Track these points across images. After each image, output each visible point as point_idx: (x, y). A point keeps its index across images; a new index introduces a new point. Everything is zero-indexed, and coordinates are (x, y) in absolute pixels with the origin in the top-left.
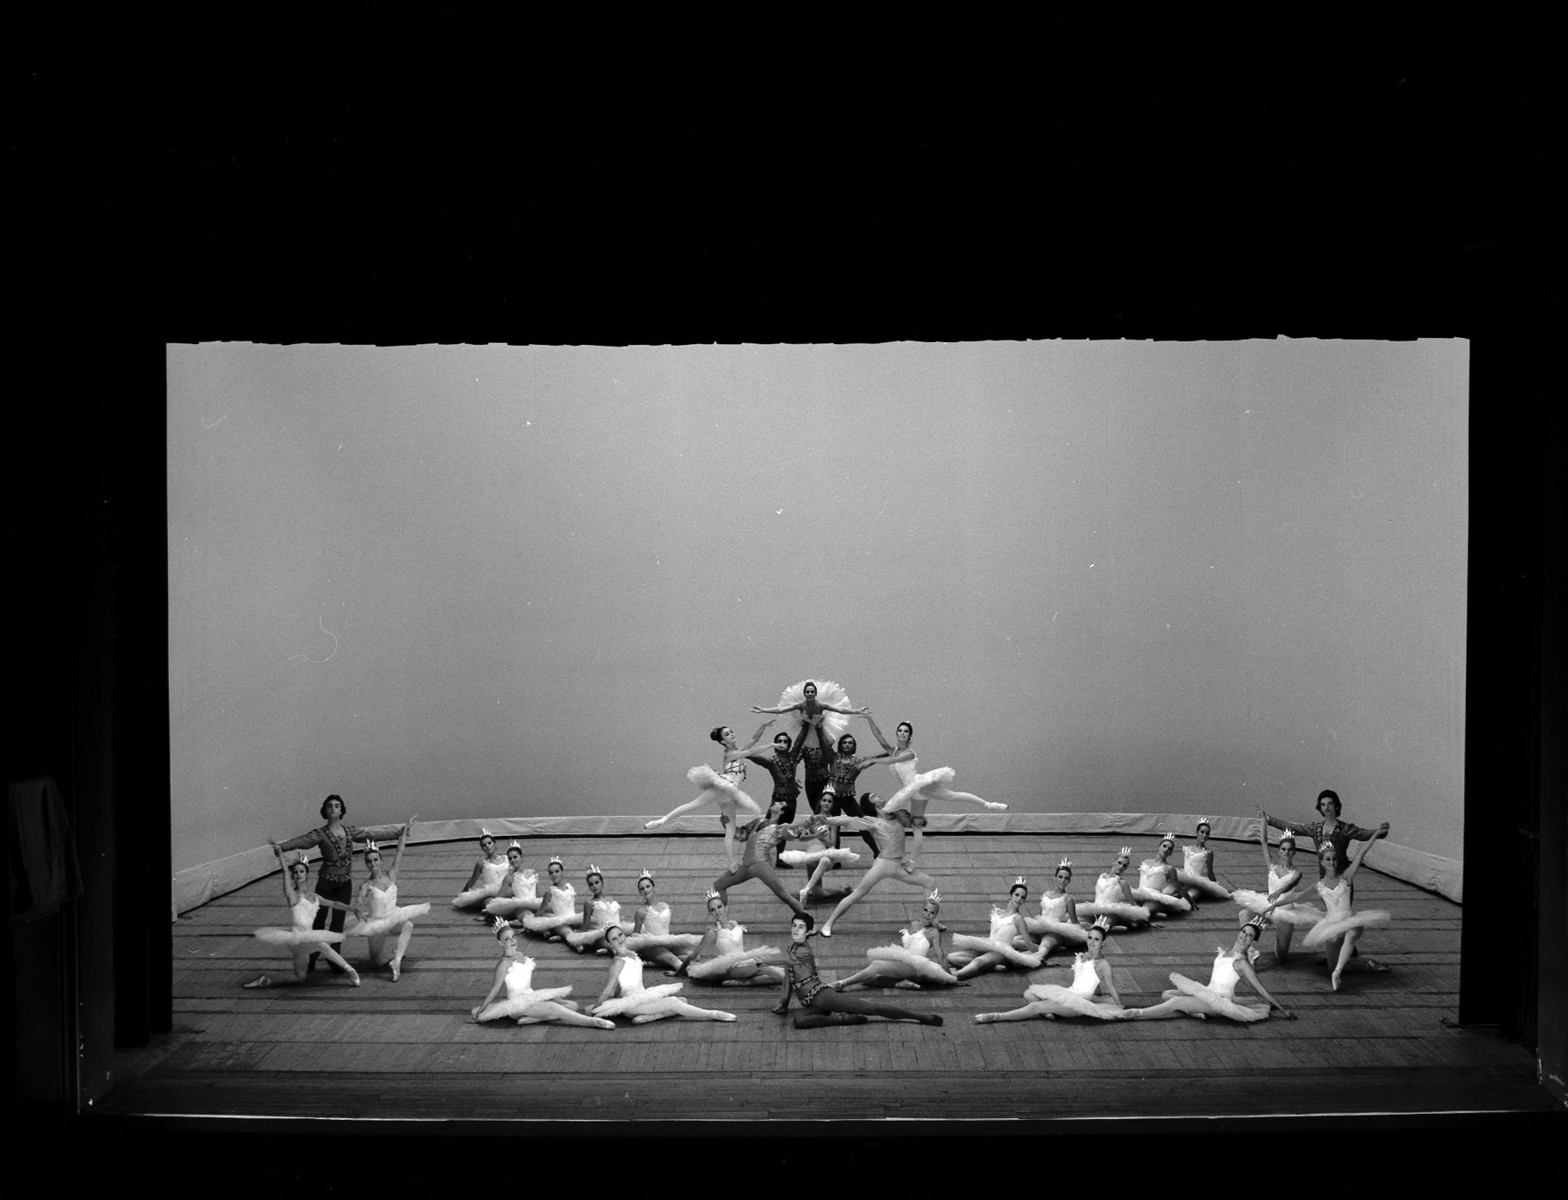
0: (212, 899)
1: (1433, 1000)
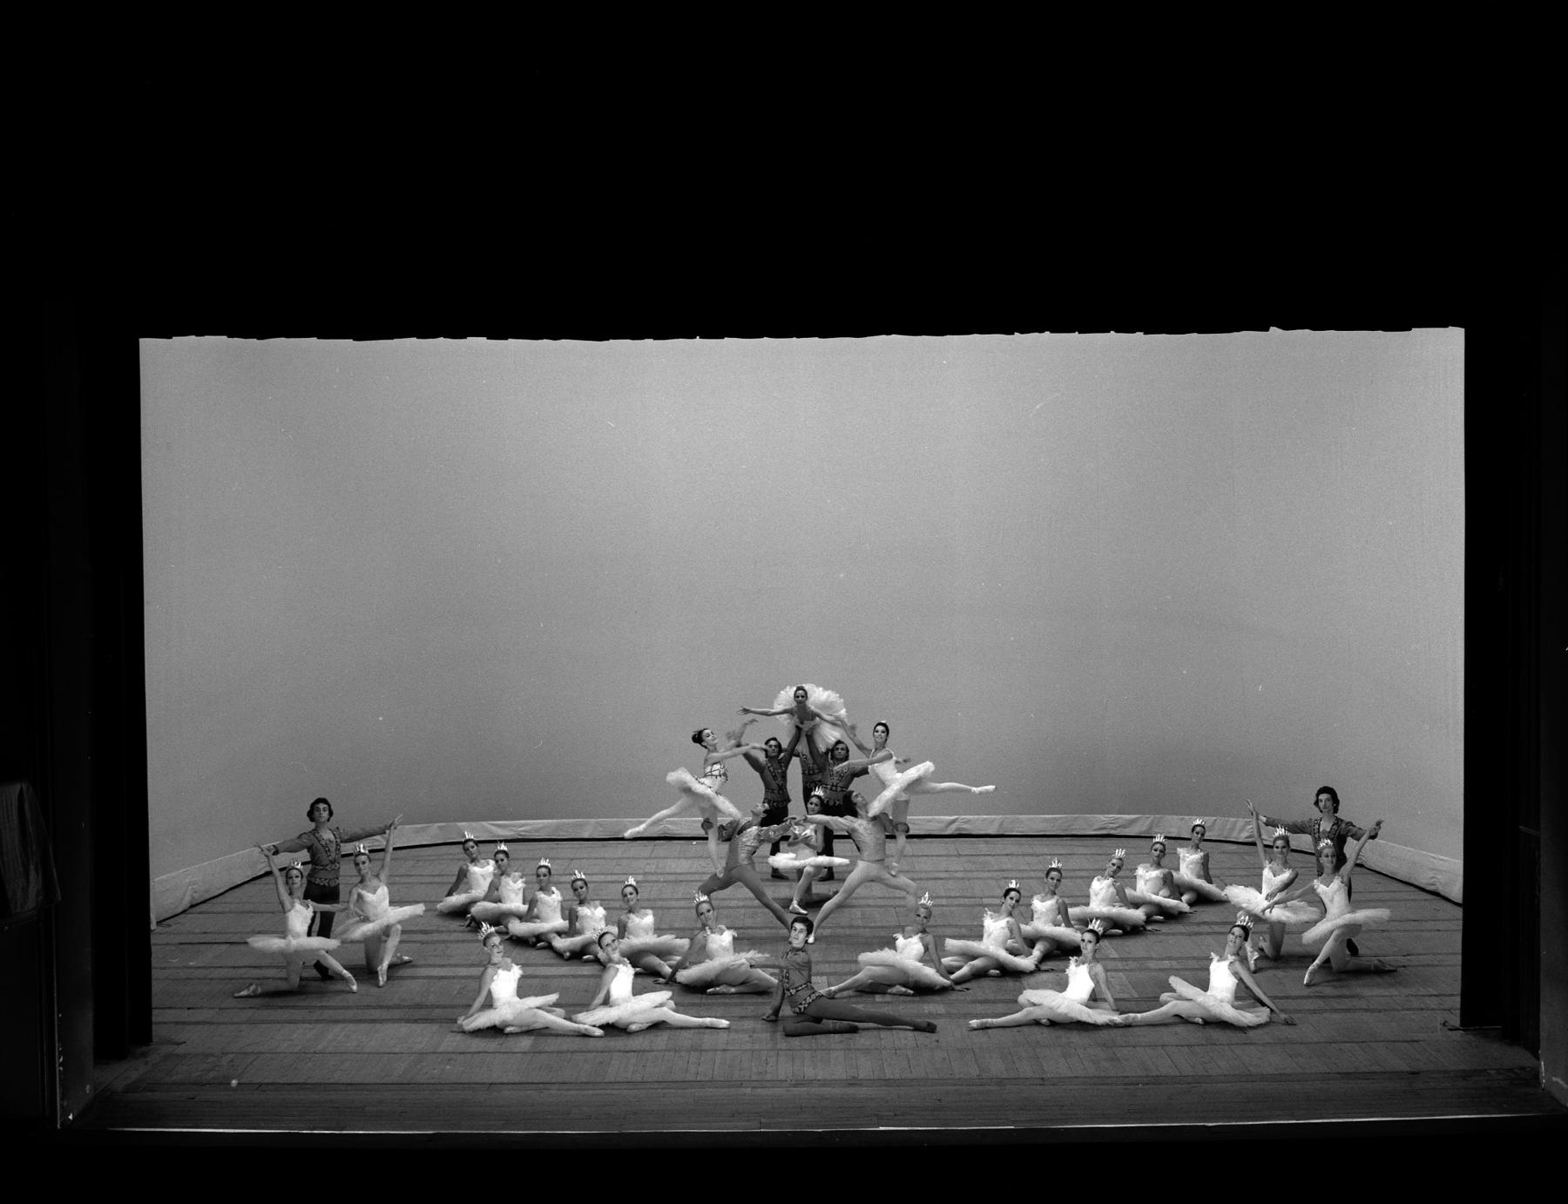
0: (192, 906)
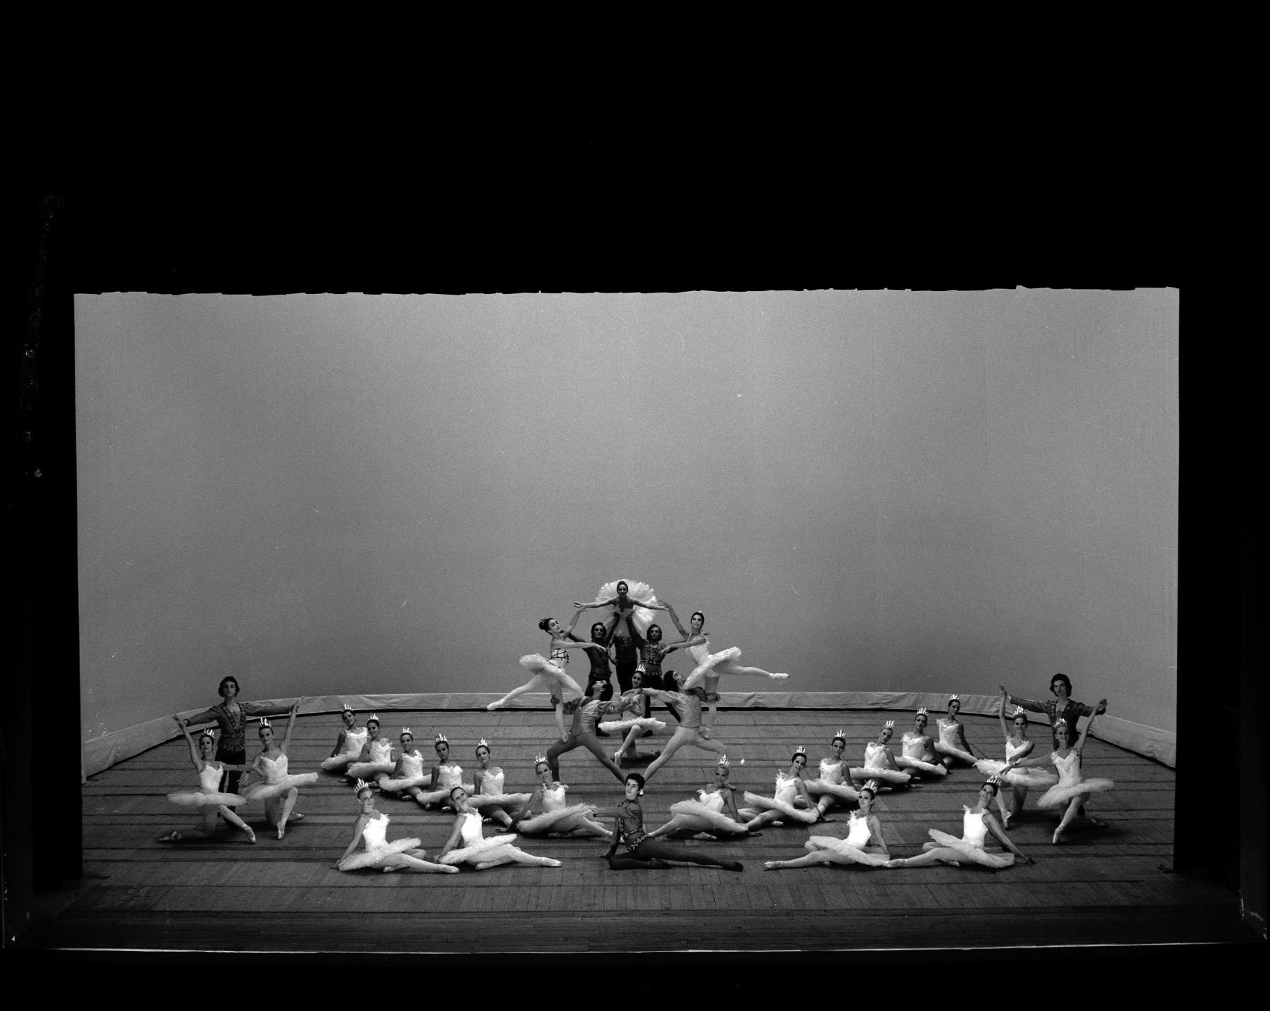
0: (116, 764)
1: (1152, 850)
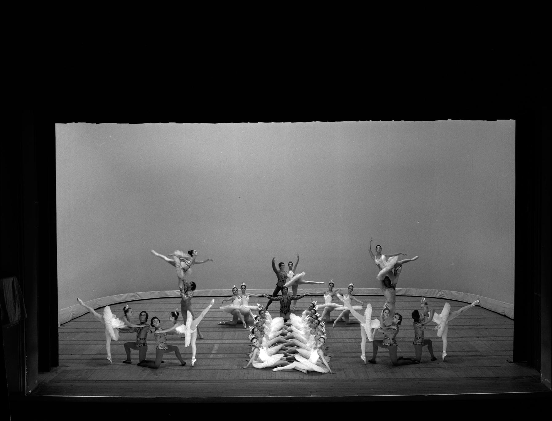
0: (306, 296)
